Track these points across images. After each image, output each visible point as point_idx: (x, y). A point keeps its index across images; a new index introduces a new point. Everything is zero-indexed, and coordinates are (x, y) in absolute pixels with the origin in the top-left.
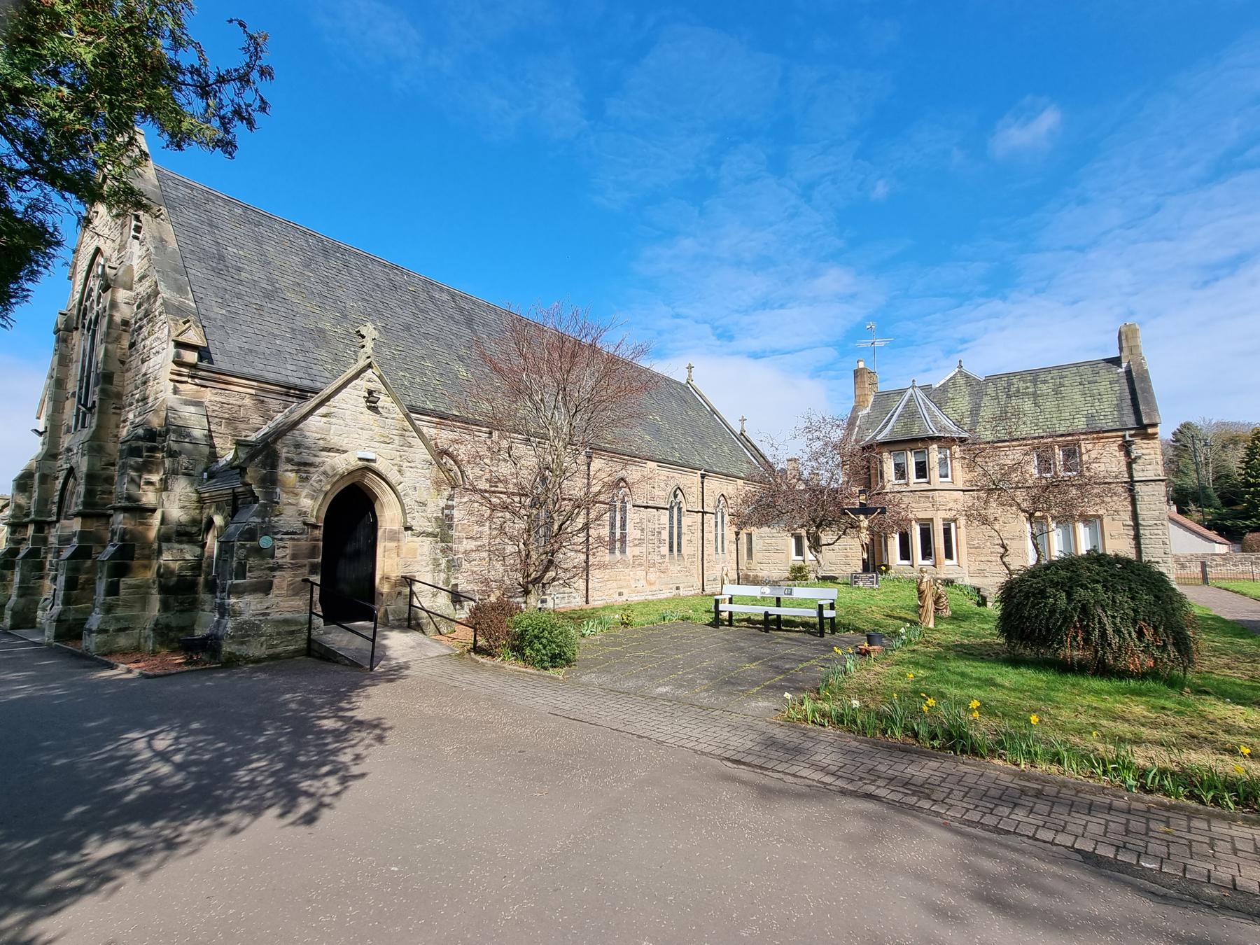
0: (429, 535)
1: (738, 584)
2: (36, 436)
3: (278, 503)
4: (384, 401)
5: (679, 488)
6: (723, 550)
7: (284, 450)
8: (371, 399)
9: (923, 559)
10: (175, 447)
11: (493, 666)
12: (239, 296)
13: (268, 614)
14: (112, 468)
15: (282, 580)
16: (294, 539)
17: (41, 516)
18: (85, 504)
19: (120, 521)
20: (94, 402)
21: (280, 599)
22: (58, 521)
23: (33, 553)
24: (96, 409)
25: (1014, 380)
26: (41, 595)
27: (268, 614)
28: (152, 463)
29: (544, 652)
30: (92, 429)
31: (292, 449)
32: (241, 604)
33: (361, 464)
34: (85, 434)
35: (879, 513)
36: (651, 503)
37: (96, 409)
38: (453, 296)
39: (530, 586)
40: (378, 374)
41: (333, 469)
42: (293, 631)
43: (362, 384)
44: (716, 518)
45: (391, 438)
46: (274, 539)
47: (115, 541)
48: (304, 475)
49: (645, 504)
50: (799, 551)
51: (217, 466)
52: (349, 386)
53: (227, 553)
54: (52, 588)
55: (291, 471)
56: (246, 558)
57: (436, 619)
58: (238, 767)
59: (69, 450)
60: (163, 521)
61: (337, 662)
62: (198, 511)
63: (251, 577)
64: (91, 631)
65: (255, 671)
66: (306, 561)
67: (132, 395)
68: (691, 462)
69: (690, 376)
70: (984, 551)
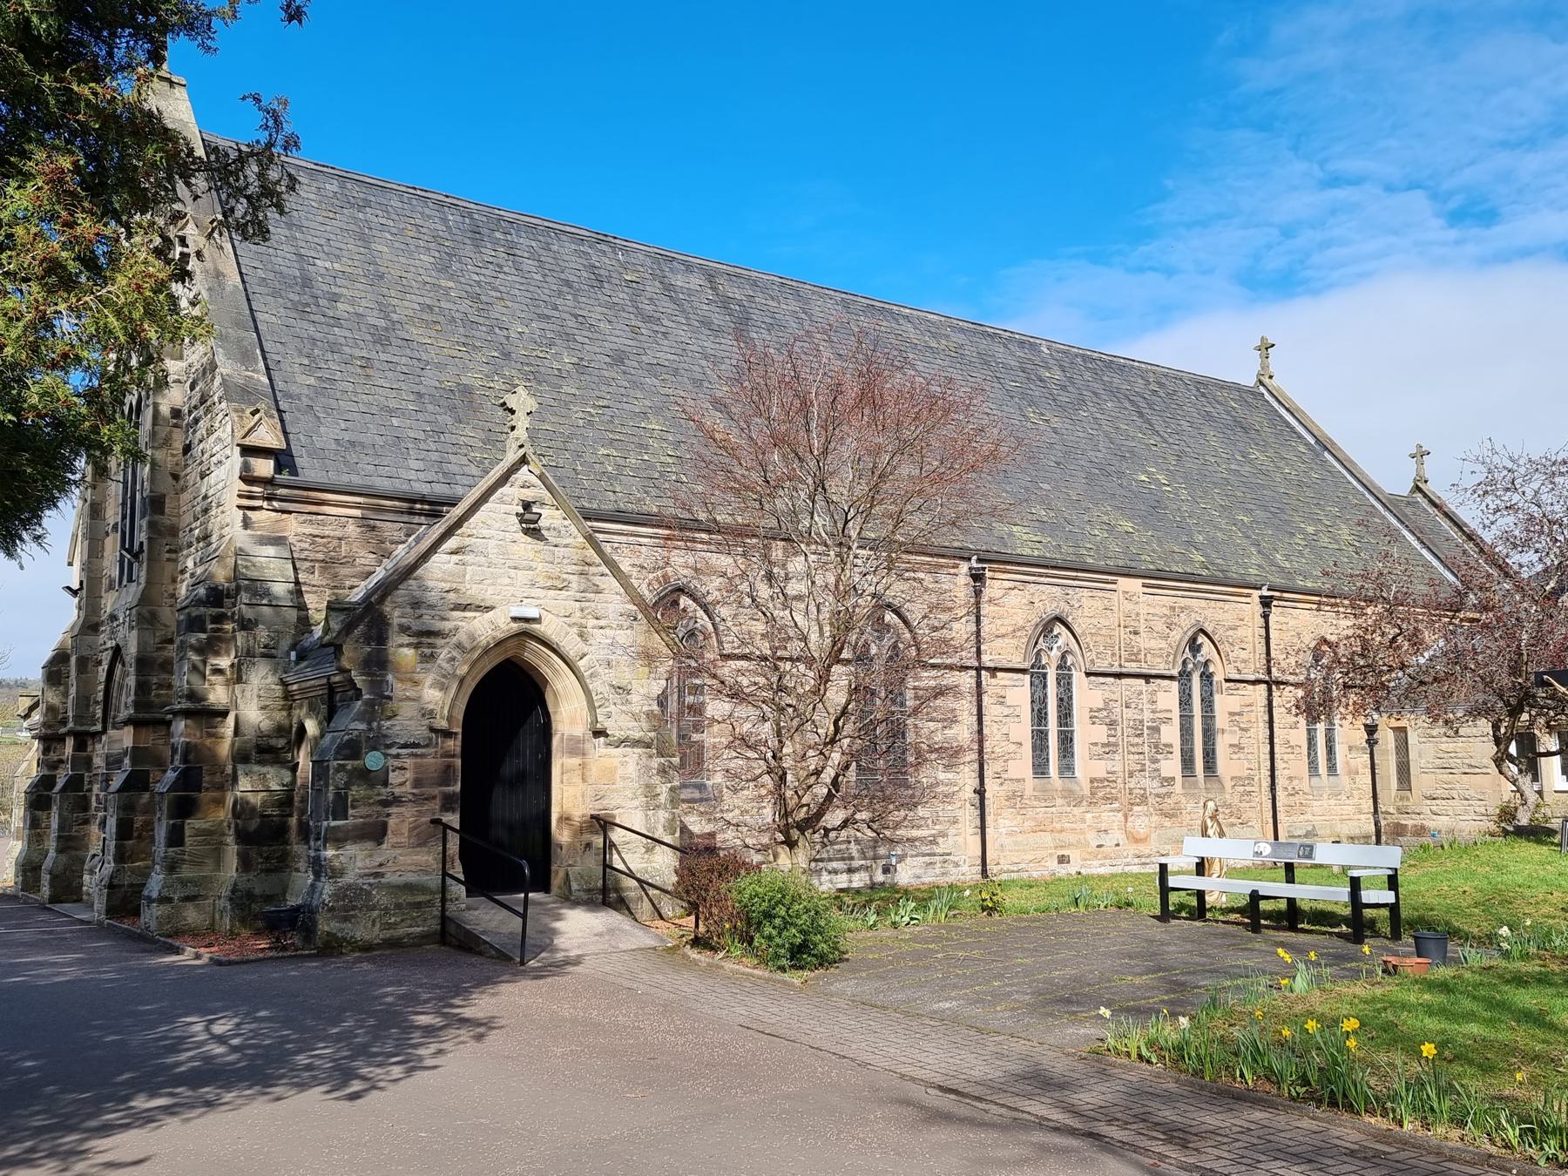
0: (637, 743)
1: (1378, 842)
2: (67, 596)
3: (390, 698)
4: (550, 517)
5: (1203, 631)
6: (1332, 769)
7: (397, 613)
8: (527, 516)
10: (248, 613)
11: (708, 964)
12: (334, 348)
13: (382, 875)
14: (171, 647)
15: (401, 821)
16: (416, 755)
17: (81, 725)
18: (137, 704)
19: (181, 729)
20: (142, 543)
21: (399, 851)
22: (104, 731)
23: (75, 783)
24: (145, 555)
26: (87, 850)
27: (382, 875)
28: (220, 639)
29: (778, 940)
30: (142, 587)
31: (409, 610)
32: (341, 858)
33: (515, 626)
34: (132, 593)
36: (1132, 667)
37: (145, 555)
38: (711, 277)
39: (795, 834)
40: (537, 472)
41: (472, 637)
42: (420, 903)
43: (512, 493)
45: (564, 580)
46: (386, 755)
47: (177, 763)
48: (427, 651)
49: (1116, 669)
51: (311, 639)
52: (491, 499)
53: (320, 779)
54: (100, 837)
55: (408, 645)
56: (348, 786)
57: (652, 892)
58: (299, 1051)
59: (113, 617)
60: (237, 731)
61: (480, 954)
62: (284, 713)
63: (354, 818)
64: (150, 900)
65: (359, 960)
66: (436, 791)
67: (191, 530)
68: (1235, 572)
69: (1264, 367)
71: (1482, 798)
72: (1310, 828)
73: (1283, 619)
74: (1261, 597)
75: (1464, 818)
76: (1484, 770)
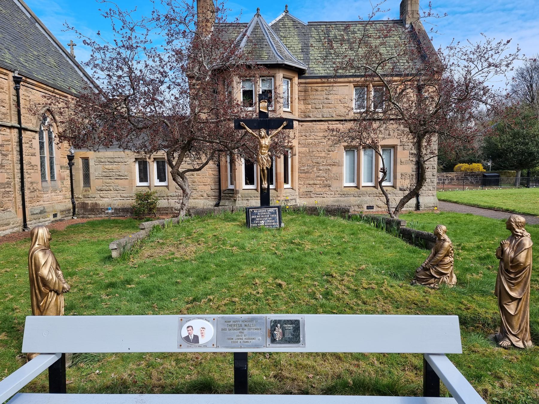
44: (41, 138)
50: (144, 177)
70: (312, 175)
71: (124, 190)
72: (42, 209)
73: (26, 94)
74: (14, 77)
75: (116, 199)
76: (125, 177)
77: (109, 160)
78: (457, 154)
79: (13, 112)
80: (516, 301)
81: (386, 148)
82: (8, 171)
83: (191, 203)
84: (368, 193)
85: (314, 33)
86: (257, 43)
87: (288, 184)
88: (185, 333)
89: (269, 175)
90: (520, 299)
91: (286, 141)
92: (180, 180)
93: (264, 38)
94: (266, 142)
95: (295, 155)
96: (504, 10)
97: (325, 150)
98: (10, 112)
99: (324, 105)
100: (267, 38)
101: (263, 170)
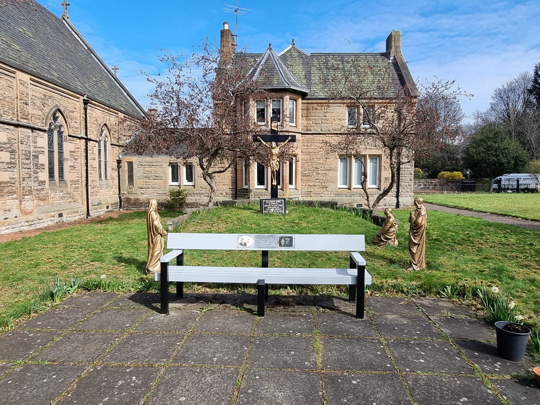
5: (59, 110)
6: (106, 177)
9: (173, 181)
25: (329, 59)
35: (289, 141)
36: (23, 122)
44: (99, 146)
49: (14, 122)
50: (175, 177)
70: (312, 178)
72: (99, 202)
73: (91, 113)
74: (84, 100)
76: (161, 178)
77: (149, 164)
78: (442, 163)
79: (82, 127)
80: (417, 246)
81: (372, 157)
82: (78, 171)
83: (216, 199)
84: (358, 193)
85: (316, 63)
86: (269, 72)
87: (292, 184)
88: (240, 242)
89: (277, 175)
90: (419, 244)
91: (291, 151)
92: (208, 179)
93: (274, 68)
94: (276, 151)
95: (299, 161)
96: (488, 35)
97: (323, 158)
98: (80, 126)
99: (322, 121)
100: (277, 67)
101: (273, 172)
